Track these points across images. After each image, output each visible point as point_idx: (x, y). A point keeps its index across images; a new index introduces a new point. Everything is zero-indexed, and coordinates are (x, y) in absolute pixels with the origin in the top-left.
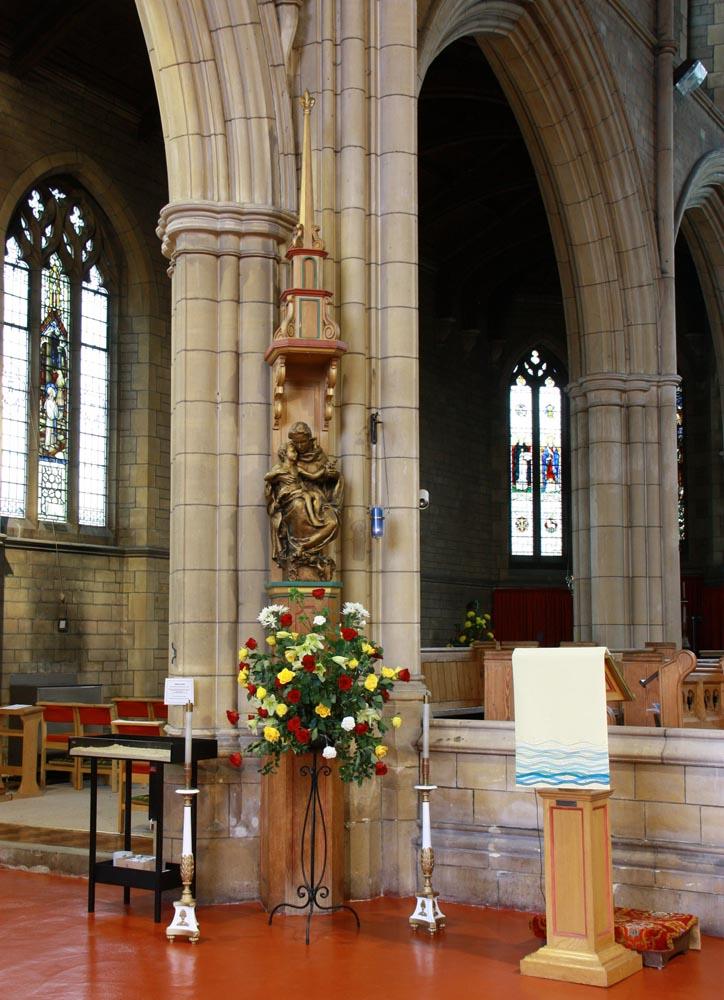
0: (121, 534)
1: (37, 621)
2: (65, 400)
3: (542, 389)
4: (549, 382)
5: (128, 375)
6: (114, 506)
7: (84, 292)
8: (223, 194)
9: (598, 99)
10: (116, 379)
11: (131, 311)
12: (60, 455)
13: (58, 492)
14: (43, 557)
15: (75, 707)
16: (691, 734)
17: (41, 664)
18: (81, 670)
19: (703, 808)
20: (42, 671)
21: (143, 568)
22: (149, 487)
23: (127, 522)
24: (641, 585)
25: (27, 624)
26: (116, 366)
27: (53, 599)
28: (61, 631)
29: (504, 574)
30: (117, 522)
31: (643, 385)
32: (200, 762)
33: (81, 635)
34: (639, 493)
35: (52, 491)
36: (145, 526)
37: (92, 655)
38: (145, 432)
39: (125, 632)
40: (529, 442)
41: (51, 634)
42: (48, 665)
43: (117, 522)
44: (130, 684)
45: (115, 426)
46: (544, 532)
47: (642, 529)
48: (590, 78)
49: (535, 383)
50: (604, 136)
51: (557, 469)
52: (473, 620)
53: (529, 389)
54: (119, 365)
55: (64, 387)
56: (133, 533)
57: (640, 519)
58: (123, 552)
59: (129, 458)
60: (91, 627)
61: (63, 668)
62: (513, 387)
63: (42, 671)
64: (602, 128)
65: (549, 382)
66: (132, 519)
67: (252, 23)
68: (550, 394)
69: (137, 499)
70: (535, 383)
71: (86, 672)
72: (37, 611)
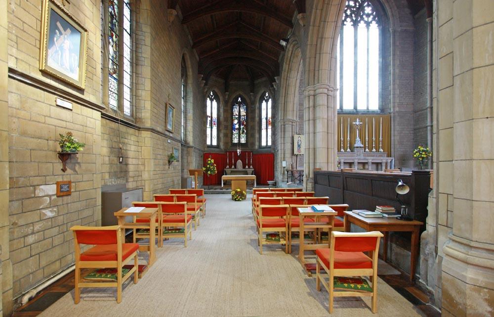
0: (137, 120)
1: (111, 157)
2: (116, 49)
4: (214, 100)
5: (140, 49)
6: (134, 108)
10: (134, 49)
11: (141, 21)
12: (114, 75)
13: (114, 94)
14: (114, 125)
15: (159, 204)
17: (113, 180)
18: (127, 182)
19: (446, 225)
20: (113, 183)
21: (149, 136)
23: (140, 115)
24: (330, 150)
25: (107, 159)
26: (134, 44)
27: (117, 147)
28: (120, 163)
29: (206, 149)
30: (136, 115)
32: (323, 237)
33: (127, 164)
34: (330, 122)
35: (112, 93)
37: (131, 174)
39: (140, 163)
40: (210, 116)
41: (117, 164)
42: (116, 180)
43: (136, 115)
44: (143, 186)
45: (135, 71)
46: (213, 138)
51: (216, 123)
52: (210, 161)
54: (136, 44)
55: (116, 42)
56: (144, 120)
57: (330, 132)
58: (140, 128)
59: (141, 87)
60: (130, 161)
61: (121, 181)
63: (113, 183)
65: (214, 100)
66: (143, 114)
68: (215, 103)
69: (146, 106)
70: (212, 100)
71: (129, 182)
72: (111, 152)
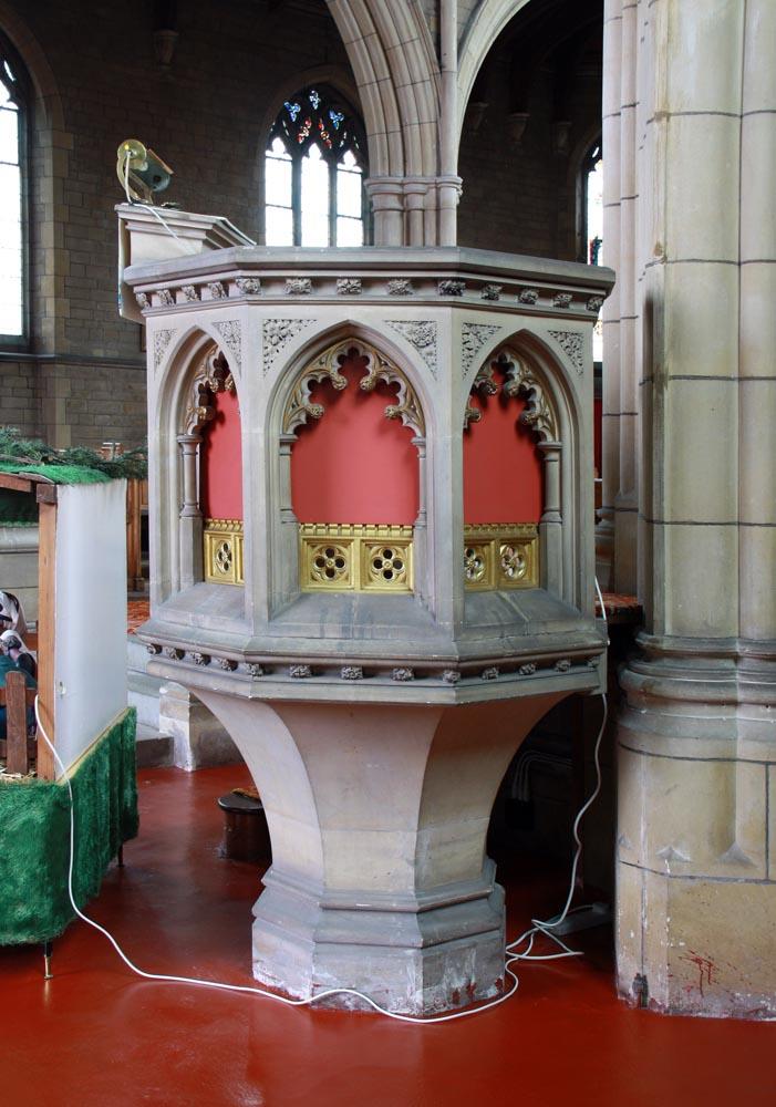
3: (304, 159)
4: (314, 150)
7: (267, 161)
8: (401, 174)
9: (395, 22)
10: (26, 193)
16: (427, 226)
22: (56, 297)
31: (421, 188)
36: (53, 335)
38: (52, 245)
47: (420, 213)
48: (403, 44)
49: (297, 151)
50: (401, 56)
53: (325, 165)
62: (268, 153)
64: (409, 89)
65: (314, 150)
66: (43, 328)
67: (663, 523)
